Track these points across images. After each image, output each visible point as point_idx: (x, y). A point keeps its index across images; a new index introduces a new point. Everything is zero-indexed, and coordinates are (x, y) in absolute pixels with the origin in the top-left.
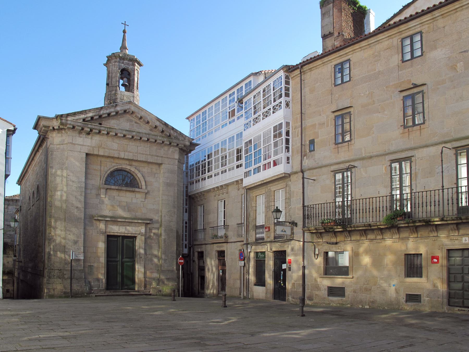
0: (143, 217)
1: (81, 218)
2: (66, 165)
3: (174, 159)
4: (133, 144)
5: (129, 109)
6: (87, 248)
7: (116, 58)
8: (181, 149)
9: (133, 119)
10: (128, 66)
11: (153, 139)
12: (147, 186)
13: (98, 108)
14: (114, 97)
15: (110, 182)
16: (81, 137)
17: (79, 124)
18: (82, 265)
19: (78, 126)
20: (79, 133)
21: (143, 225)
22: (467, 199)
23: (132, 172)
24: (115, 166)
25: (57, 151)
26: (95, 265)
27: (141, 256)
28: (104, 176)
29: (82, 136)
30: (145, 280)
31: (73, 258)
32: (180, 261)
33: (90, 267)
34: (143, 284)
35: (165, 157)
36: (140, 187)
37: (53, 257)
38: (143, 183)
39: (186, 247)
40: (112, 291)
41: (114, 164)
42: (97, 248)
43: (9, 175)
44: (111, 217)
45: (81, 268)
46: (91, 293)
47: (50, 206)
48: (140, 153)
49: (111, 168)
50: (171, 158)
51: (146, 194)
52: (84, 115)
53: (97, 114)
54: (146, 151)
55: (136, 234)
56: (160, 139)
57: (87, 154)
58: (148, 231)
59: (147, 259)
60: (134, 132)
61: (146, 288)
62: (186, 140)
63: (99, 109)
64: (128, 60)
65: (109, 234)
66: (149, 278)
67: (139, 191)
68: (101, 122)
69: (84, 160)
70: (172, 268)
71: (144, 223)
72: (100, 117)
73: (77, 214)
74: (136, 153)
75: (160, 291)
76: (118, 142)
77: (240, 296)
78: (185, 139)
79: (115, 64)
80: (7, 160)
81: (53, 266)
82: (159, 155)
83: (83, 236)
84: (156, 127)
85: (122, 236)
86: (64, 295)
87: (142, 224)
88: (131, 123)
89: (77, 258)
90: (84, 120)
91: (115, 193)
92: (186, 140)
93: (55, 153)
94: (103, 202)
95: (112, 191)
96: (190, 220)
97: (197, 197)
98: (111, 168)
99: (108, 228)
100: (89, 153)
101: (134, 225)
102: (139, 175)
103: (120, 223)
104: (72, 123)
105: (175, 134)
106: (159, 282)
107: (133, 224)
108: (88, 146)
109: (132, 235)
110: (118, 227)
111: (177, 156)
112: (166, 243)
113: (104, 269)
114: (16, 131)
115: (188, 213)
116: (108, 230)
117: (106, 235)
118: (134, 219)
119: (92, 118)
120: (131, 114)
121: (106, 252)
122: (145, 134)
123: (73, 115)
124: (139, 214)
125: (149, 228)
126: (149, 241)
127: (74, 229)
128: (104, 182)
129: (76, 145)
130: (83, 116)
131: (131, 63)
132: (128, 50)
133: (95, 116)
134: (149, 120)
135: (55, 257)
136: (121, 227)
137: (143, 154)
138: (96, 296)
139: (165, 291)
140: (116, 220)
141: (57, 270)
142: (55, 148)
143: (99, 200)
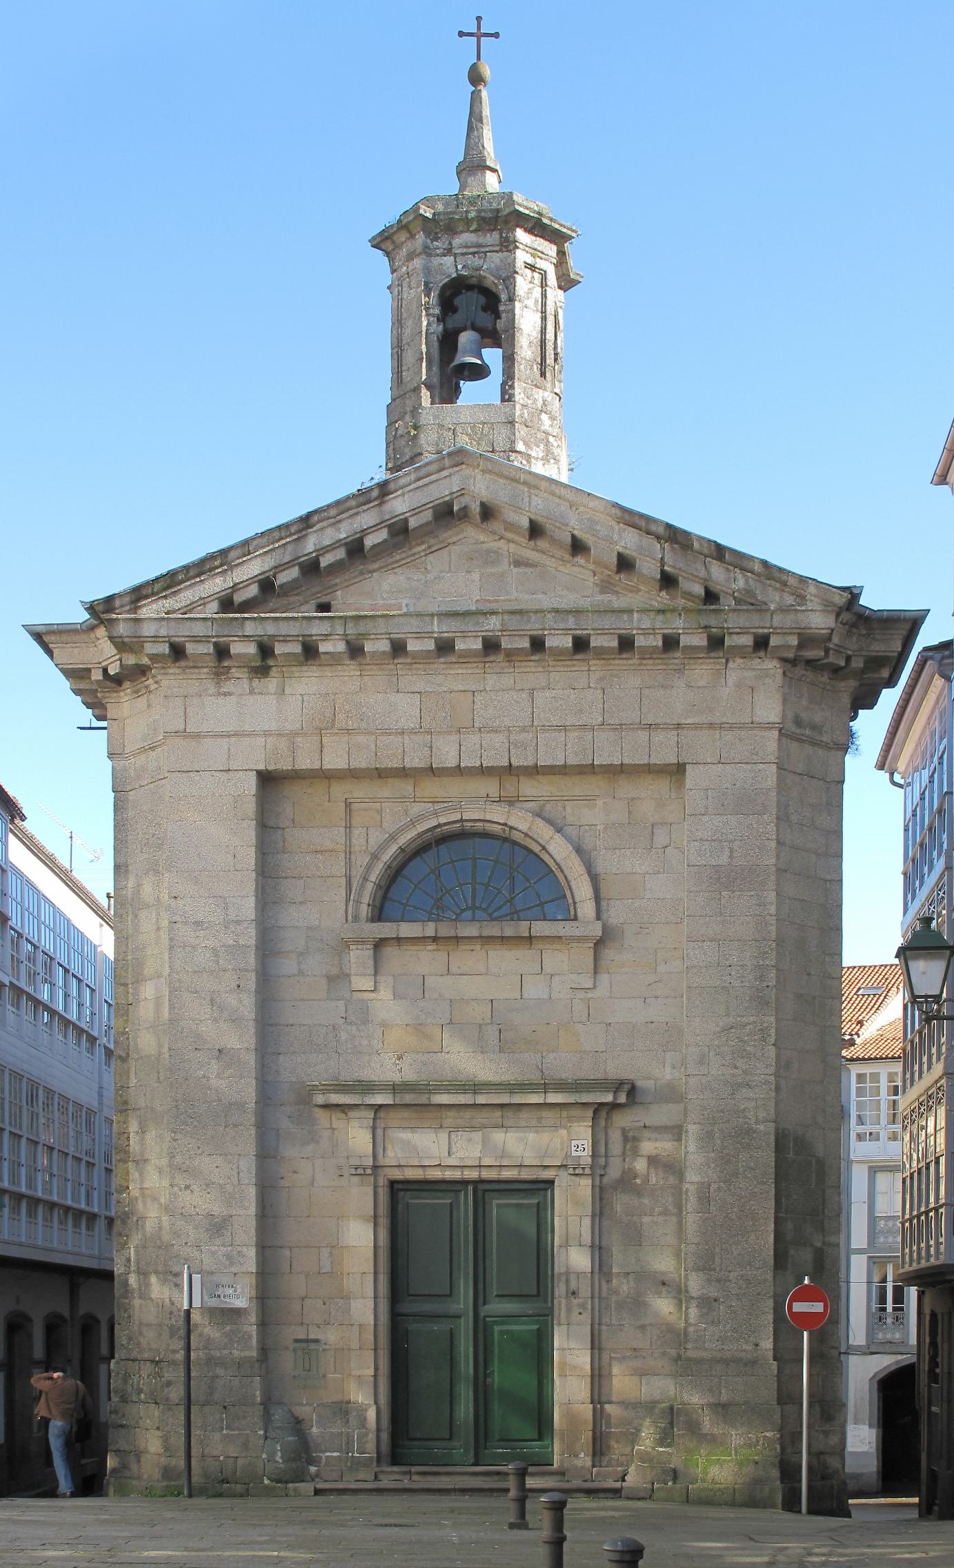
0: (587, 1071)
1: (241, 1106)
3: (754, 725)
4: (507, 680)
5: (462, 493)
6: (287, 1253)
7: (412, 236)
9: (496, 544)
10: (475, 261)
11: (602, 632)
12: (604, 904)
13: (286, 526)
14: (407, 450)
15: (406, 905)
16: (225, 694)
17: (199, 629)
18: (250, 1337)
19: (196, 639)
20: (217, 674)
21: (581, 1119)
23: (516, 836)
24: (421, 818)
26: (331, 1336)
27: (573, 1285)
28: (365, 879)
29: (232, 689)
30: (599, 1415)
31: (197, 1303)
34: (586, 1437)
35: (696, 727)
37: (137, 1302)
38: (582, 890)
40: (414, 1469)
41: (416, 809)
42: (336, 1248)
44: (395, 1088)
45: (247, 1353)
46: (300, 1477)
48: (546, 728)
49: (401, 830)
50: (732, 727)
51: (599, 944)
52: (219, 580)
53: (287, 559)
56: (646, 624)
57: (267, 780)
58: (616, 1147)
59: (614, 1298)
60: (493, 613)
61: (605, 1460)
62: (810, 606)
63: (293, 529)
64: (474, 227)
65: (397, 1175)
66: (624, 1404)
68: (324, 600)
69: (250, 807)
70: (749, 1347)
72: (311, 568)
73: (222, 1084)
74: (524, 729)
75: (675, 1475)
76: (420, 686)
78: (802, 598)
81: (139, 1344)
83: (252, 1192)
84: (625, 564)
85: (477, 1183)
86: (165, 1483)
87: (576, 1112)
88: (490, 570)
89: (213, 1303)
90: (227, 604)
91: (426, 961)
92: (810, 606)
94: (364, 1015)
95: (409, 952)
98: (401, 830)
99: (389, 1147)
100: (271, 768)
101: (534, 1123)
102: (559, 850)
103: (451, 1113)
104: (163, 632)
105: (740, 576)
106: (671, 1423)
107: (525, 1114)
108: (267, 734)
110: (444, 1136)
111: (769, 708)
112: (713, 1208)
113: (370, 1355)
116: (390, 1153)
118: (522, 1087)
119: (267, 585)
122: (557, 611)
123: (165, 589)
124: (563, 1064)
126: (620, 1203)
127: (207, 1159)
128: (364, 910)
129: (209, 740)
130: (216, 584)
131: (492, 238)
132: (494, 171)
133: (279, 568)
134: (576, 532)
135: (143, 1302)
136: (460, 1139)
137: (565, 728)
138: (317, 1492)
139: (705, 1473)
140: (423, 1099)
141: (148, 1364)
143: (341, 1004)
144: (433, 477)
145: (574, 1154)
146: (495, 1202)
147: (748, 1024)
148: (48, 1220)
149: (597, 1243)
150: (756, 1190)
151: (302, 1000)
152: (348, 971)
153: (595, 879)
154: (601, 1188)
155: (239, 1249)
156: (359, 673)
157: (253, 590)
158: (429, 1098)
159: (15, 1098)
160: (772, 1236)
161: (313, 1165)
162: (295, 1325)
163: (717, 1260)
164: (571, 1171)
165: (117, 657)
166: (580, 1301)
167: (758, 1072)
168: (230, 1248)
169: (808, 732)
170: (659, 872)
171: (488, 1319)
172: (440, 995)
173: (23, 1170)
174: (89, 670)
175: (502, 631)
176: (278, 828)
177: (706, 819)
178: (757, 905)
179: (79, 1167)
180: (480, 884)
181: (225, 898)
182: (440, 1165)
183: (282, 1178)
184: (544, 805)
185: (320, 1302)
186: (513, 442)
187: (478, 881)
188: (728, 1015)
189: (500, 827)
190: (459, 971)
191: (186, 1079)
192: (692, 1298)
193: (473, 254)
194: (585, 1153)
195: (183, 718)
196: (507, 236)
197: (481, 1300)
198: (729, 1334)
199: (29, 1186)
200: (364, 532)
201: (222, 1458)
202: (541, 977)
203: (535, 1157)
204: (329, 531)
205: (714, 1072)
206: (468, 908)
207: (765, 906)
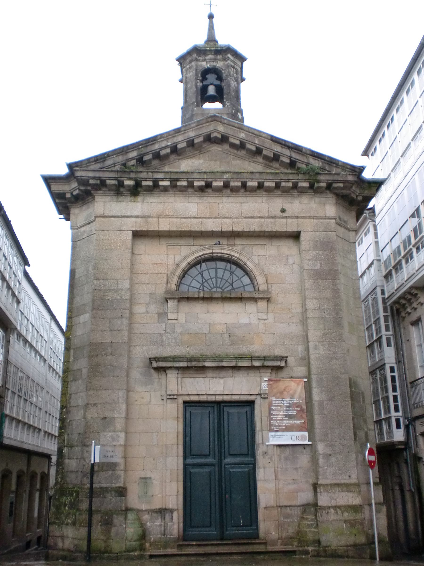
10: (214, 64)
39: (398, 427)
54: (260, 211)
55: (251, 395)
65: (187, 398)
77: (370, 532)
100: (138, 229)
140: (200, 364)
143: (164, 325)
144: (204, 125)
145: (264, 388)
148: (23, 429)
150: (343, 404)
151: (147, 323)
152: (166, 311)
159: (15, 377)
161: (150, 395)
163: (329, 436)
165: (77, 187)
167: (339, 353)
169: (343, 223)
171: (226, 466)
173: (15, 407)
175: (231, 179)
177: (310, 252)
179: (36, 409)
181: (117, 280)
182: (206, 394)
185: (152, 459)
187: (218, 277)
190: (212, 312)
192: (320, 454)
193: (213, 61)
197: (223, 457)
198: (337, 471)
199: (17, 415)
200: (177, 143)
202: (246, 314)
205: (321, 353)
206: (214, 287)
207: (336, 285)
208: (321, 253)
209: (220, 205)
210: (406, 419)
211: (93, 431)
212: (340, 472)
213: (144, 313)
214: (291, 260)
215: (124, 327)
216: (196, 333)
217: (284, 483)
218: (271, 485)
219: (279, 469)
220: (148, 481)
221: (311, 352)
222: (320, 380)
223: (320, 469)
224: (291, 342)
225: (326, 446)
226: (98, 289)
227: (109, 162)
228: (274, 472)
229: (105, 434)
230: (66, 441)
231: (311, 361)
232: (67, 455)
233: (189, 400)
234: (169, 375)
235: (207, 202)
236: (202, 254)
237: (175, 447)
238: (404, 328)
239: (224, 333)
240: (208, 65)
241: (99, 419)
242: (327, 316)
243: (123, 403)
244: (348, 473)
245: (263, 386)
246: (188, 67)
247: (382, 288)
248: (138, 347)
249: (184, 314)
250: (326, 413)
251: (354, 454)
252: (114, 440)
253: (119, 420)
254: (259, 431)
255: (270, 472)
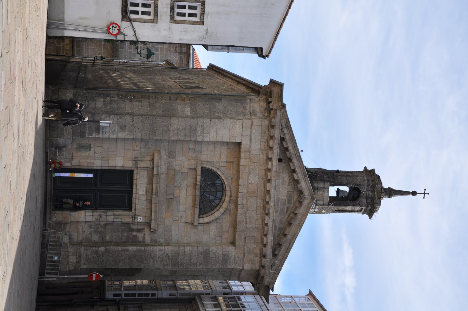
2: (223, 118)
4: (259, 205)
8: (258, 272)
12: (203, 225)
22: (170, 302)
23: (221, 204)
25: (242, 107)
32: (94, 276)
33: (89, 147)
35: (244, 249)
36: (201, 216)
39: (115, 295)
43: (207, 49)
47: (171, 98)
51: (192, 224)
54: (250, 222)
57: (239, 144)
64: (373, 196)
65: (135, 172)
67: (196, 214)
71: (151, 221)
72: (290, 160)
79: (365, 180)
80: (226, 47)
82: (246, 241)
93: (239, 104)
96: (158, 300)
97: (193, 307)
100: (242, 146)
102: (217, 214)
109: (133, 205)
114: (262, 58)
115: (168, 297)
117: (133, 169)
120: (299, 201)
121: (110, 168)
125: (144, 229)
128: (205, 166)
142: (245, 105)
145: (138, 218)
146: (127, 195)
147: (169, 261)
149: (114, 222)
150: (126, 263)
153: (209, 223)
154: (129, 223)
155: (116, 133)
156: (264, 169)
157: (285, 146)
158: (154, 183)
160: (114, 268)
162: (95, 144)
164: (134, 217)
166: (99, 219)
167: (157, 264)
168: (116, 131)
170: (210, 238)
171: (95, 193)
172: (182, 184)
174: (272, 98)
176: (227, 145)
177: (221, 251)
178: (199, 263)
180: (210, 193)
181: (210, 133)
182: (137, 184)
183: (135, 142)
184: (228, 210)
185: (101, 151)
186: (318, 206)
188: (172, 256)
189: (224, 200)
190: (188, 189)
191: (162, 122)
192: (98, 248)
194: (138, 220)
195: (256, 124)
196: (369, 204)
198: (88, 257)
201: (57, 127)
203: (138, 208)
204: (298, 166)
208: (221, 258)
209: (255, 198)
210: (120, 300)
211: (118, 120)
212: (88, 259)
213: (189, 147)
214: (218, 239)
215: (179, 138)
216: (174, 179)
217: (83, 226)
218: (82, 219)
219: (91, 224)
220: (88, 149)
221: (159, 248)
222: (141, 251)
223: (90, 248)
224: (166, 235)
225: (103, 252)
226: (204, 122)
227: (286, 131)
228: (90, 221)
229: (116, 127)
230: (114, 99)
231: (153, 247)
232: (106, 100)
233: (134, 174)
234: (149, 163)
235: (258, 189)
236: (226, 184)
237: (107, 165)
238: (179, 306)
239: (174, 195)
240: (363, 193)
241: (125, 123)
242: (180, 258)
243: (134, 137)
244: (86, 263)
245: (140, 218)
246: (365, 178)
247: (211, 294)
248: (168, 143)
249: (187, 172)
250: (122, 253)
251: (97, 268)
252: (113, 131)
253: (124, 134)
254: (114, 213)
255: (89, 219)
